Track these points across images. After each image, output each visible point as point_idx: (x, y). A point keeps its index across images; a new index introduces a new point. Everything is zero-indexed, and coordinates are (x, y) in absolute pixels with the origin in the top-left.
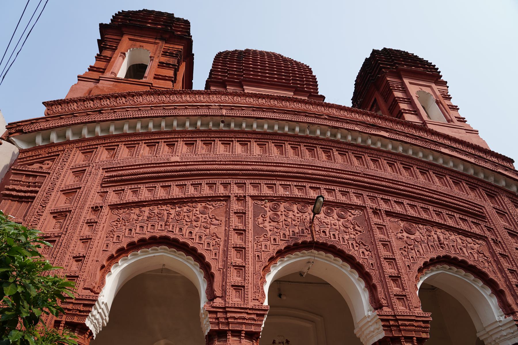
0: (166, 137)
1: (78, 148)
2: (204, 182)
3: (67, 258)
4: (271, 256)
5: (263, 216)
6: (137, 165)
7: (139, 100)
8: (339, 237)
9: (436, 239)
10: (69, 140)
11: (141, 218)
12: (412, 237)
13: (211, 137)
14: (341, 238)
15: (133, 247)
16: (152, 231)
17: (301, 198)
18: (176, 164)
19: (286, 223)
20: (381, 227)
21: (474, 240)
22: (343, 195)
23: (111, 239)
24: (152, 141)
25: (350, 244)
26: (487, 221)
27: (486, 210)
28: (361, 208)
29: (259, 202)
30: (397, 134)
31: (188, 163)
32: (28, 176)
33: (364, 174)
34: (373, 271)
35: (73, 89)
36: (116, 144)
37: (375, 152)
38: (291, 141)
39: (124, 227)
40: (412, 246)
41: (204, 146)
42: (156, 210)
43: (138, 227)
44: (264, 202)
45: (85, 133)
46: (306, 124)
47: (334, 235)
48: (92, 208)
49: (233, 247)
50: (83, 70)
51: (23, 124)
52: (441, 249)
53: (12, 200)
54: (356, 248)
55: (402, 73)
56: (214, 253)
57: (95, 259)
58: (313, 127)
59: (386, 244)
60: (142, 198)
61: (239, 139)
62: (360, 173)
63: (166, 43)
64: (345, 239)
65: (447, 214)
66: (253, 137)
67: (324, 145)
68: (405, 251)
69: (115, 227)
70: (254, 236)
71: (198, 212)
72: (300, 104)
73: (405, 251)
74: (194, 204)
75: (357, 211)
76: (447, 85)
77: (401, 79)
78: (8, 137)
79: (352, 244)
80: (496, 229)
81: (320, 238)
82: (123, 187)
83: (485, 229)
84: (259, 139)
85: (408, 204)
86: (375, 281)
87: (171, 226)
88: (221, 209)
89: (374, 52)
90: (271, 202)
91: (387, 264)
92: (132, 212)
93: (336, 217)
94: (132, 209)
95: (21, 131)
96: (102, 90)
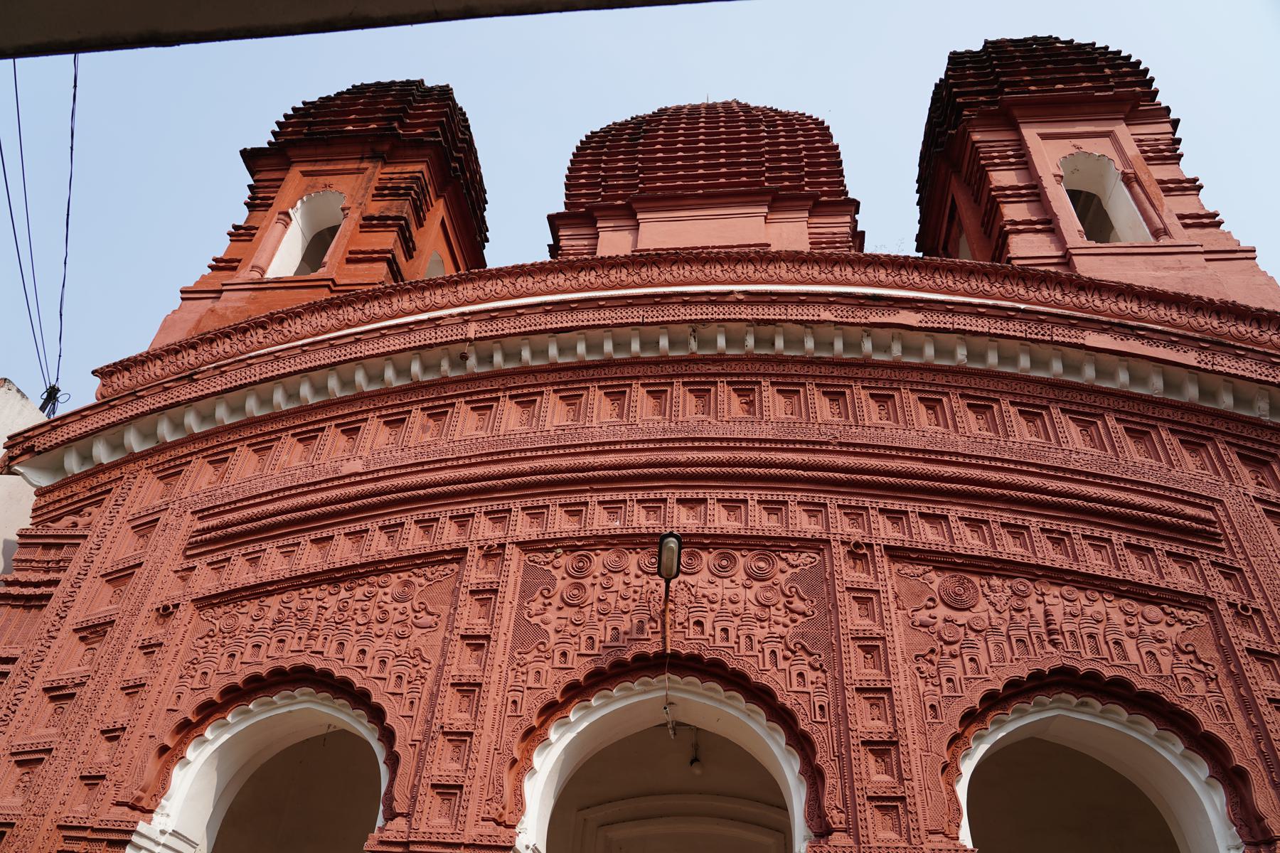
0: (341, 413)
1: (151, 468)
2: (409, 519)
3: (87, 735)
4: (546, 702)
5: (545, 592)
6: (266, 494)
7: (292, 329)
8: (738, 637)
9: (1040, 618)
10: (132, 454)
11: (258, 625)
12: (962, 617)
13: (445, 398)
14: (743, 639)
15: (235, 696)
16: (277, 655)
17: (649, 534)
18: (353, 479)
19: (602, 606)
20: (864, 598)
21: (1169, 610)
22: (770, 511)
23: (190, 680)
24: (310, 428)
25: (767, 652)
26: (1223, 545)
27: (1225, 509)
28: (817, 545)
29: (540, 557)
30: (950, 311)
31: (381, 474)
32: (47, 547)
33: (841, 444)
34: (821, 728)
35: (167, 325)
36: (230, 447)
37: (886, 374)
38: (649, 377)
39: (221, 650)
40: (956, 647)
41: (431, 423)
42: (295, 600)
43: (250, 646)
44: (551, 556)
45: (166, 432)
46: (685, 326)
47: (725, 630)
48: (158, 610)
49: (453, 685)
50: (196, 270)
51: (37, 432)
52: (1050, 648)
53: (13, 607)
54: (783, 665)
55: (1016, 112)
56: (408, 702)
57: (149, 731)
58: (705, 331)
59: (871, 647)
60: (266, 576)
61: (514, 393)
62: (827, 443)
63: (386, 163)
64: (755, 640)
65: (1085, 537)
66: (551, 380)
67: (738, 375)
68: (931, 662)
69: (201, 651)
70: (513, 649)
71: (388, 599)
72: (688, 267)
73: (931, 662)
74: (381, 579)
75: (804, 555)
76: (1173, 116)
77: (1017, 130)
78: (9, 467)
79: (773, 652)
80: (1253, 571)
81: (682, 642)
82: (228, 553)
83: (1212, 572)
84: (566, 383)
85: (961, 519)
86: (823, 758)
87: (321, 638)
88: (443, 585)
89: (956, 60)
90: (572, 551)
91: (866, 704)
92: (243, 610)
93: (741, 577)
94: (245, 602)
95: (30, 450)
96: (223, 316)
